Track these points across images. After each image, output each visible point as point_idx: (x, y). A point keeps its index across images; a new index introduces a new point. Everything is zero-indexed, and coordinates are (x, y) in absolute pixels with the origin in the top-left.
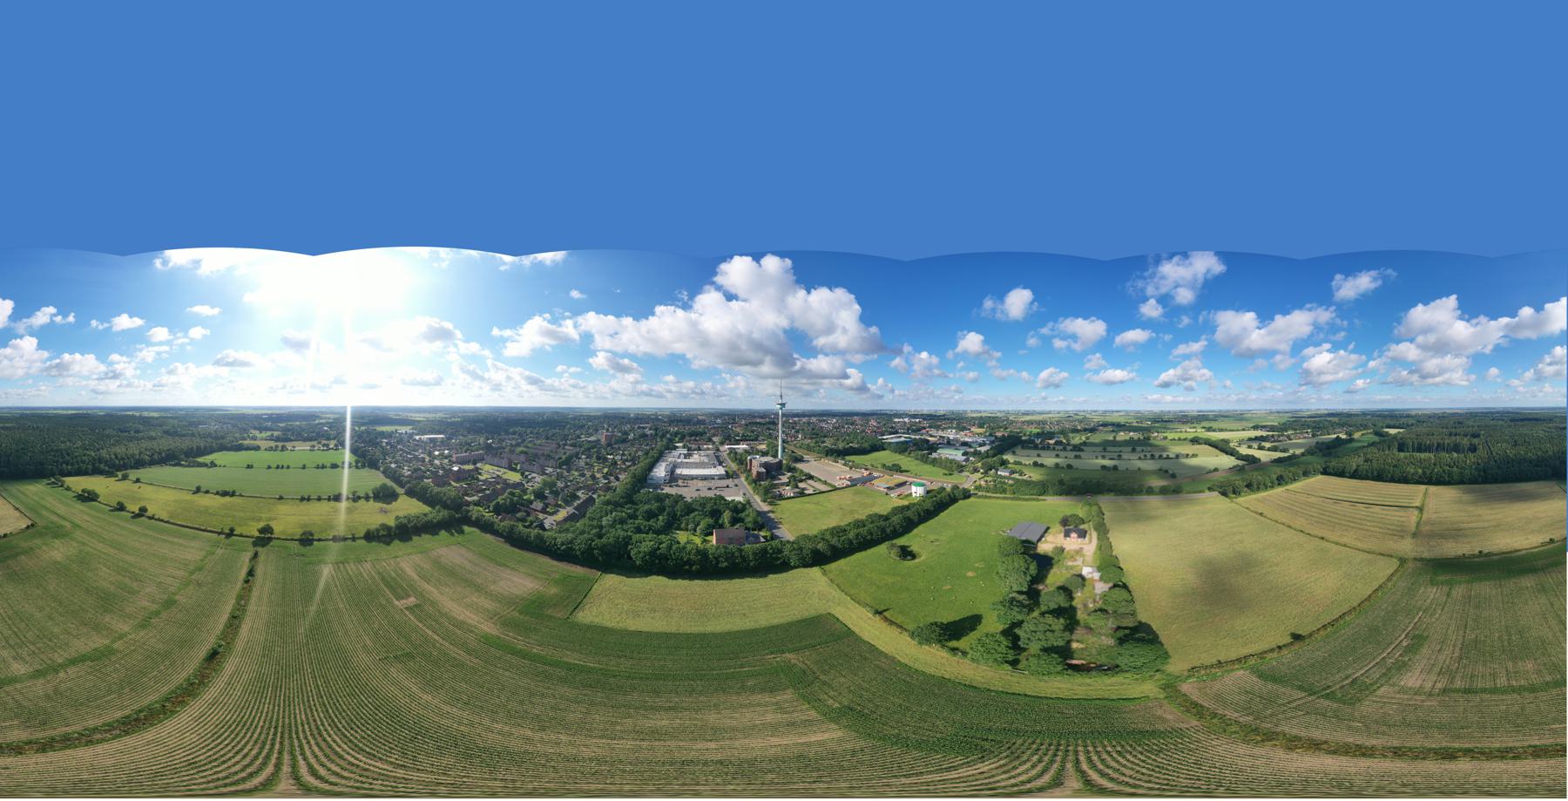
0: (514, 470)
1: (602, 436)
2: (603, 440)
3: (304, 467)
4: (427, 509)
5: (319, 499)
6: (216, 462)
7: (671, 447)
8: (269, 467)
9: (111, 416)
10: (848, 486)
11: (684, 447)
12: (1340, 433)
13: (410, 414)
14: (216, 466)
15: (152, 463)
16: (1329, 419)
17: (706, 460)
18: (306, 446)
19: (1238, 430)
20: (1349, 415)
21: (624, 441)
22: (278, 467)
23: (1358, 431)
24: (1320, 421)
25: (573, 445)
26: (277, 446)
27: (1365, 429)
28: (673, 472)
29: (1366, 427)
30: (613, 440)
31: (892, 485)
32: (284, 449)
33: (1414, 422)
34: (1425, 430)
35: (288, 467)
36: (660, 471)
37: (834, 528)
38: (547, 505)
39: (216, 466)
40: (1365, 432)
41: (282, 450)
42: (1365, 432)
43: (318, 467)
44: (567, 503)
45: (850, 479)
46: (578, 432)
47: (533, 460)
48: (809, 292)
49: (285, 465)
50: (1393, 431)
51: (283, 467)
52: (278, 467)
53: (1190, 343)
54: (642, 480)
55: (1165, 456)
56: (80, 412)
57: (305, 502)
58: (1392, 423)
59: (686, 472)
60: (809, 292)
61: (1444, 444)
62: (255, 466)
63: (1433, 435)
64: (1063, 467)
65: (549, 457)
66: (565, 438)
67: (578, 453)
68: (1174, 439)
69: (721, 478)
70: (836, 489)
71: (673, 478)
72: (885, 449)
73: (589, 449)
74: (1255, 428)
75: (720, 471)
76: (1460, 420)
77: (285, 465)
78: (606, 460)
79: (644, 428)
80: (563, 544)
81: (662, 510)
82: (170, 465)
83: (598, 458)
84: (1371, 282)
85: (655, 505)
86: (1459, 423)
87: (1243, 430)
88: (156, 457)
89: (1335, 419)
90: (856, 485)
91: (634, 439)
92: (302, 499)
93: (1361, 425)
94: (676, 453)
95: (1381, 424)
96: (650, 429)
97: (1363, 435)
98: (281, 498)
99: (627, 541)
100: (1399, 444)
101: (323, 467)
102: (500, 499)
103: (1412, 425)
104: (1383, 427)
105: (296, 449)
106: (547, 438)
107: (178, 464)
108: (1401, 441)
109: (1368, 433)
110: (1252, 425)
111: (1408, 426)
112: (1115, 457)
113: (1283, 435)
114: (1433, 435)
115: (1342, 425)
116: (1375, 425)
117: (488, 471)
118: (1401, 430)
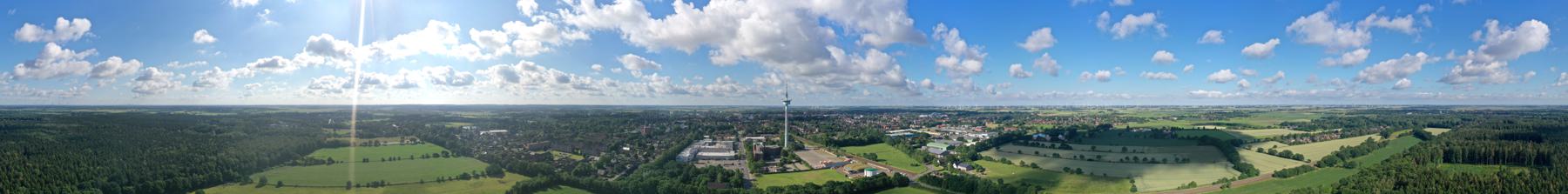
0: (577, 154)
1: (643, 130)
2: (644, 133)
3: (412, 158)
4: (527, 178)
5: (450, 179)
6: (334, 159)
7: (700, 137)
8: (383, 160)
9: (164, 115)
10: (823, 168)
11: (710, 138)
12: (1374, 132)
13: (458, 113)
14: (333, 162)
15: (273, 164)
16: (1367, 116)
17: (724, 147)
18: (395, 141)
19: (1262, 128)
20: (1389, 112)
21: (662, 133)
22: (390, 159)
23: (1396, 130)
24: (1355, 119)
25: (620, 136)
26: (370, 142)
27: (1404, 128)
28: (695, 156)
29: (1405, 126)
30: (652, 133)
31: (855, 169)
32: (377, 144)
33: (1459, 120)
34: (1475, 131)
35: (399, 159)
36: (687, 154)
37: (774, 187)
38: (607, 173)
39: (333, 162)
40: (1403, 132)
41: (376, 145)
42: (1403, 132)
43: (423, 157)
44: (620, 171)
45: (826, 164)
46: (622, 127)
47: (590, 147)
48: (701, 10)
49: (397, 157)
50: (1436, 132)
51: (394, 159)
52: (390, 159)
53: (1034, 33)
54: (673, 157)
55: (1149, 159)
56: (129, 111)
57: (442, 183)
58: (1435, 122)
59: (705, 154)
60: (701, 10)
61: (1504, 153)
62: (370, 160)
63: (1485, 138)
64: (1027, 166)
65: (601, 144)
66: (611, 131)
67: (624, 142)
68: (1183, 138)
69: (731, 158)
70: (812, 169)
71: (695, 158)
72: (882, 142)
73: (632, 139)
74: (1283, 125)
75: (732, 153)
76: (1510, 119)
77: (397, 157)
78: (645, 146)
79: (680, 123)
80: (621, 186)
81: (680, 173)
82: (289, 165)
83: (640, 145)
84: (849, 26)
85: (676, 170)
86: (1510, 122)
87: (1269, 127)
88: (273, 156)
89: (1374, 116)
90: (829, 168)
91: (671, 132)
92: (439, 181)
93: (1400, 124)
94: (702, 142)
95: (1422, 123)
96: (685, 124)
97: (1400, 136)
98: (422, 182)
99: (656, 183)
100: (1445, 152)
101: (428, 157)
102: (576, 168)
103: (1458, 124)
104: (1424, 126)
105: (389, 143)
106: (596, 131)
107: (294, 164)
108: (1447, 148)
109: (1407, 134)
110: (1281, 122)
111: (1453, 125)
112: (1095, 158)
113: (1307, 135)
114: (1485, 138)
115: (1378, 123)
116: (1415, 124)
117: (557, 155)
118: (1446, 130)
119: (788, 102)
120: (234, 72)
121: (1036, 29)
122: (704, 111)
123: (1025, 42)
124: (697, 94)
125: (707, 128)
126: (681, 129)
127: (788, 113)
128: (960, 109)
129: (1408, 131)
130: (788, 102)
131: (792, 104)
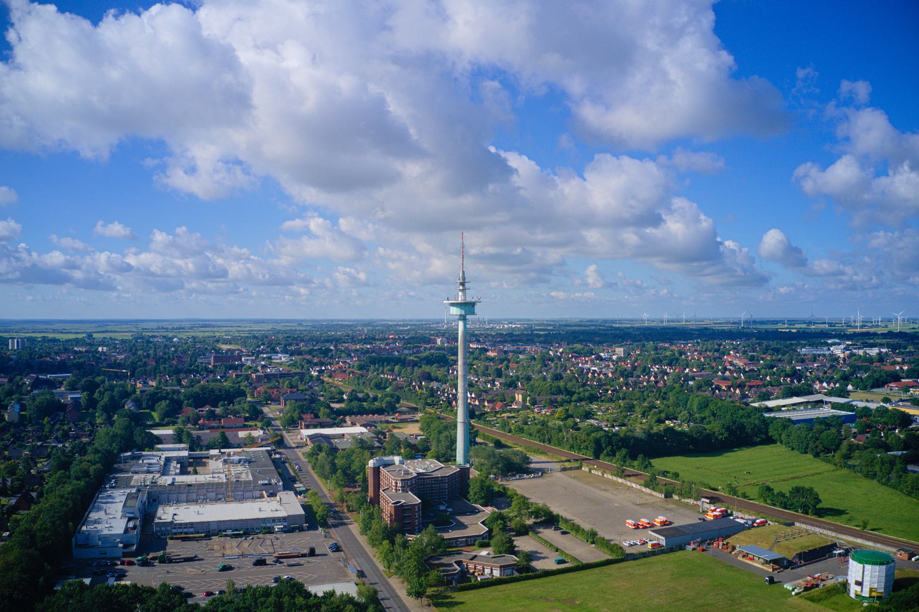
10: (657, 551)
11: (178, 438)
17: (245, 474)
31: (790, 556)
45: (666, 529)
69: (291, 526)
79: (52, 384)
90: (681, 548)
96: (73, 388)
119: (468, 307)
120: (73, 259)
121: (75, 14)
122: (119, 336)
123: (608, 107)
124: (94, 284)
125: (154, 399)
126: (63, 407)
127: (467, 341)
128: (897, 328)
129: (183, 445)
130: (468, 307)
131: (483, 313)
